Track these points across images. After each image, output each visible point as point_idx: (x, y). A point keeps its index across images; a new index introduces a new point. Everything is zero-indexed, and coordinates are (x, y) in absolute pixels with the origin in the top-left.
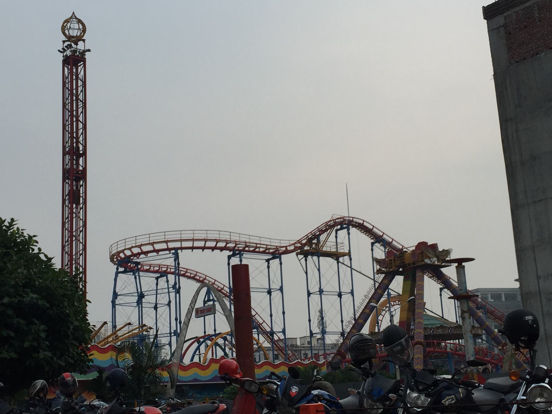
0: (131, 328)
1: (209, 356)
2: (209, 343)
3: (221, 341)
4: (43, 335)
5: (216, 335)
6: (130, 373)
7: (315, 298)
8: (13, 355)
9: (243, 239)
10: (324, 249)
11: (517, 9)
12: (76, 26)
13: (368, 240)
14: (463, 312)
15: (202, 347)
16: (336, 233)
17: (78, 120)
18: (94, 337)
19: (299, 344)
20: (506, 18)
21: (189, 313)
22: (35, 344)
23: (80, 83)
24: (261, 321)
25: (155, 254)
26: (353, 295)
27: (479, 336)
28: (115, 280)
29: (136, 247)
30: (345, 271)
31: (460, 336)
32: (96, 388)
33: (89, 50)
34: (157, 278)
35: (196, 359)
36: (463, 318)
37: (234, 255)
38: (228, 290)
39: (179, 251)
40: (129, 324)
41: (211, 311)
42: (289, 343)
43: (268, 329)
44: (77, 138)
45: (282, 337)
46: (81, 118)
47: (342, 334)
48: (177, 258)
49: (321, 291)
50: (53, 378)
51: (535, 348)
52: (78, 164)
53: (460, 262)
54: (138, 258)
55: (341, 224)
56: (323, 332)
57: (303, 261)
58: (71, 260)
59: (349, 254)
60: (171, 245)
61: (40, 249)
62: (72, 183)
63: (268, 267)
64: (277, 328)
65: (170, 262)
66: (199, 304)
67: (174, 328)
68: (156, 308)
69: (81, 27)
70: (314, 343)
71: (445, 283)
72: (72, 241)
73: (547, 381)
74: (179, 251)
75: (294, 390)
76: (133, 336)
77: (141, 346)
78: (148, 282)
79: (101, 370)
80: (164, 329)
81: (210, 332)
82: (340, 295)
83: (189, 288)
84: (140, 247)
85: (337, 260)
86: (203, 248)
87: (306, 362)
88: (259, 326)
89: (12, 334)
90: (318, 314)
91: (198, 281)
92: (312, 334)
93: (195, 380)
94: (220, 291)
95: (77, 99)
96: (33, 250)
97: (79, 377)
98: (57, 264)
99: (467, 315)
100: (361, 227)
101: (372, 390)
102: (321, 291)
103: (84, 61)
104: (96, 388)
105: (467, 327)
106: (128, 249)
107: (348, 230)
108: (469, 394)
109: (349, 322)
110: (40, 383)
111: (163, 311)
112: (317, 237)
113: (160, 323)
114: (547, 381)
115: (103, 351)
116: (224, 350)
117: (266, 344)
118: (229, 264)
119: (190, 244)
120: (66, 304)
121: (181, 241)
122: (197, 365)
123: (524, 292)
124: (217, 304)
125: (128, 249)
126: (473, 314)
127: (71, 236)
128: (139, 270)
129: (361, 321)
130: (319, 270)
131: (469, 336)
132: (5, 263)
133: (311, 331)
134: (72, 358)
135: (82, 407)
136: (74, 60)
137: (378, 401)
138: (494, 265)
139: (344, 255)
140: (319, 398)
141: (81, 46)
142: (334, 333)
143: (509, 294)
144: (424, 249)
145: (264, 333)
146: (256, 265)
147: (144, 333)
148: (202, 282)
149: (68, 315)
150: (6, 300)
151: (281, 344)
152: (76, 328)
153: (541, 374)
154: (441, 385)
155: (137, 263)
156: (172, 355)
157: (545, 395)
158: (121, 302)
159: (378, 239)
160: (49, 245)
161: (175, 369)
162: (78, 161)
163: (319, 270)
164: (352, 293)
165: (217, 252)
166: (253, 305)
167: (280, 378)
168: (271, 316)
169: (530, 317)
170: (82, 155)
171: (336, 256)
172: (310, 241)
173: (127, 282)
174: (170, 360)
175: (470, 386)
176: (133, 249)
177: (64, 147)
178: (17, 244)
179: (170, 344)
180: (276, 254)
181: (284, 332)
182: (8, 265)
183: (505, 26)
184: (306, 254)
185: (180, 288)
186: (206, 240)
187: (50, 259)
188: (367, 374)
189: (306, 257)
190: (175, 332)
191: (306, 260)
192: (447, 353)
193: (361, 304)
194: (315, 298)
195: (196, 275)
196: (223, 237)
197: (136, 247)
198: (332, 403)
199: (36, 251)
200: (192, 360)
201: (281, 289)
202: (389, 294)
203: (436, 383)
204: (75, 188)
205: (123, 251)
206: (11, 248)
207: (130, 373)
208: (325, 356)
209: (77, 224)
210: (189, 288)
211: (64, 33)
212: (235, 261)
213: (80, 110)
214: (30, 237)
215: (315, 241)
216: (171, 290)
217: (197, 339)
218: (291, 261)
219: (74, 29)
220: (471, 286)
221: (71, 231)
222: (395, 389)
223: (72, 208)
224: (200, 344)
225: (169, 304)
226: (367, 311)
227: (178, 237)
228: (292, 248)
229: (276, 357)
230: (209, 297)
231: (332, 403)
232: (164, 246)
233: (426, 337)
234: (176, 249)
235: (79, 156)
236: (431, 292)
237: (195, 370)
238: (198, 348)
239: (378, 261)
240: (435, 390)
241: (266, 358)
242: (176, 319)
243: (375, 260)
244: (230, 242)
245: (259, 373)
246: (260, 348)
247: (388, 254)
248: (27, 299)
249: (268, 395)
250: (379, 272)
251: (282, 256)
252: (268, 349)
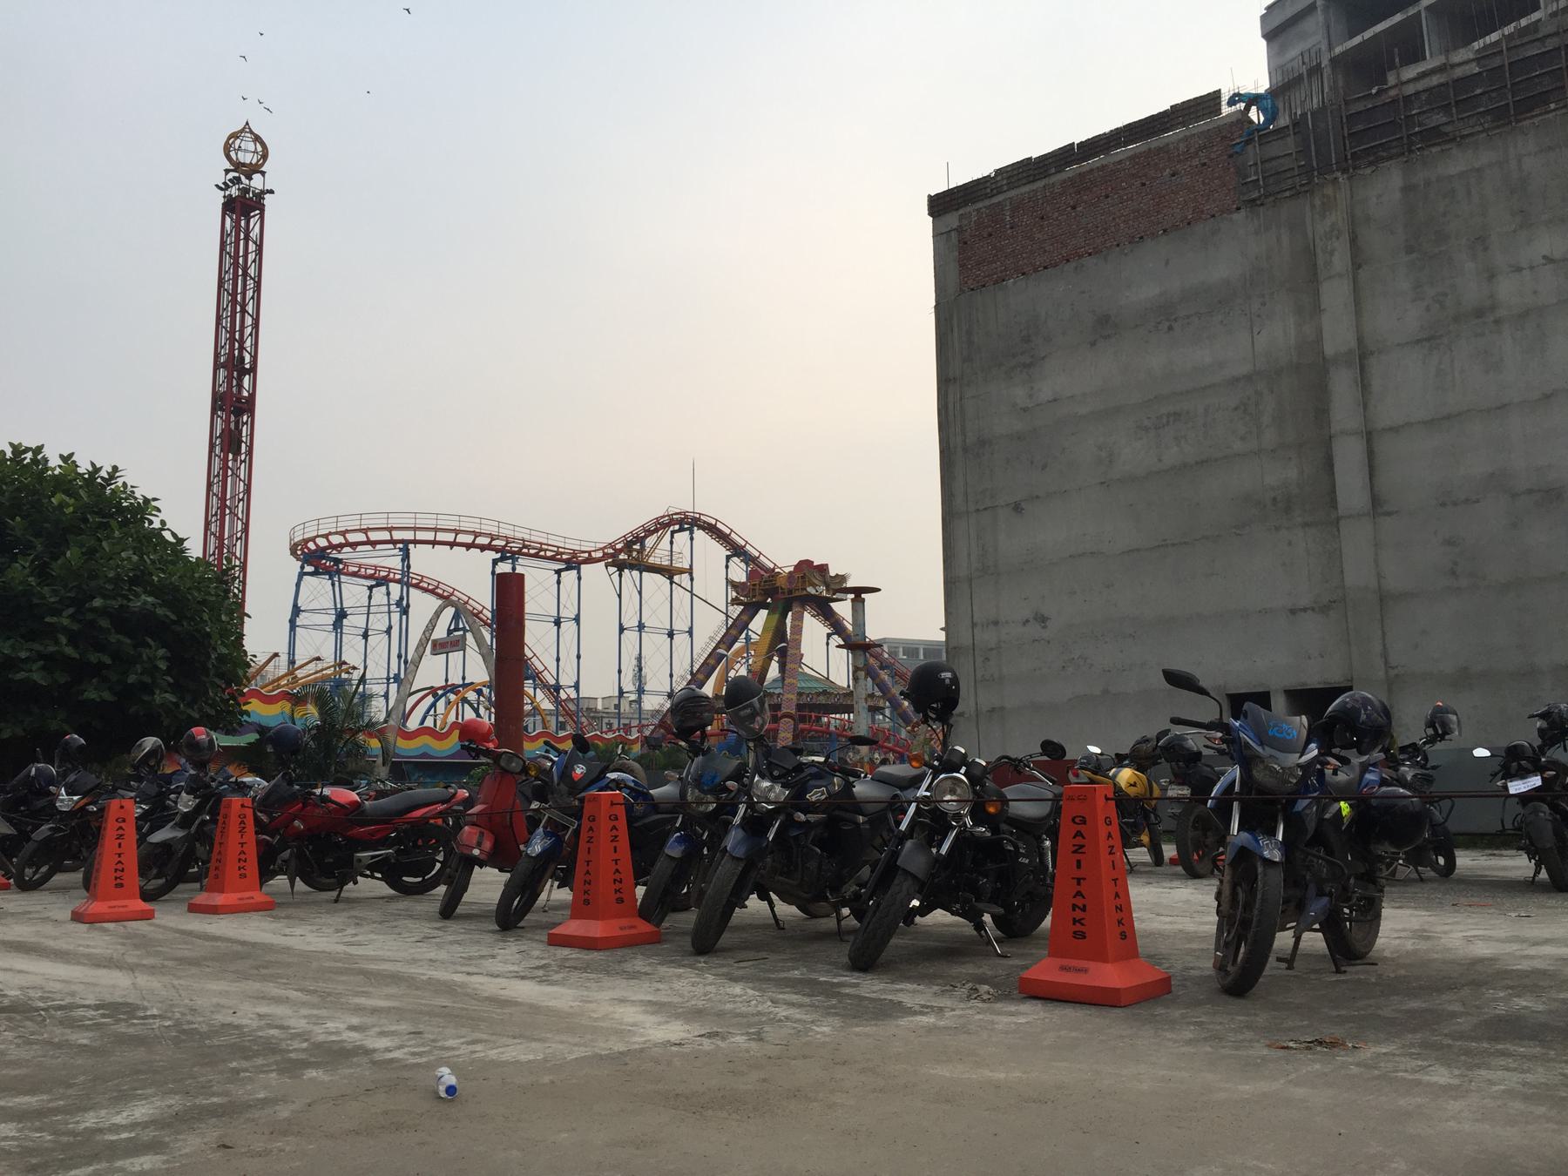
0: (320, 665)
1: (452, 718)
2: (452, 697)
3: (472, 696)
4: (163, 666)
5: (465, 686)
6: (314, 738)
7: (631, 637)
8: (107, 696)
10: (651, 560)
11: (980, 205)
12: (251, 146)
13: (722, 552)
14: (856, 669)
15: (441, 704)
17: (244, 311)
18: (254, 677)
19: (600, 707)
20: (961, 217)
21: (421, 646)
22: (147, 679)
23: (252, 247)
24: (541, 668)
25: (369, 547)
27: (880, 710)
28: (298, 585)
29: (360, 530)
30: (681, 596)
31: (849, 709)
32: (251, 758)
33: (271, 192)
34: (371, 588)
35: (429, 722)
36: (856, 679)
37: (502, 559)
38: (489, 615)
39: (411, 546)
40: (318, 659)
41: (459, 645)
42: (584, 705)
43: (552, 682)
44: (242, 342)
45: (573, 695)
46: (250, 308)
47: (670, 695)
48: (406, 556)
49: (641, 627)
50: (175, 738)
51: (951, 721)
52: (240, 386)
53: (859, 592)
55: (681, 522)
56: (641, 691)
57: (616, 577)
58: (220, 547)
59: (690, 571)
60: (397, 535)
61: (163, 523)
62: (228, 418)
63: (559, 582)
64: (567, 680)
65: (395, 562)
66: (440, 633)
67: (394, 670)
68: (365, 636)
69: (259, 148)
70: (625, 707)
71: (836, 626)
72: (223, 515)
73: (963, 770)
74: (411, 546)
75: (580, 770)
76: (325, 679)
77: (336, 698)
78: (354, 592)
79: (262, 730)
80: (377, 671)
81: (456, 679)
82: (671, 635)
83: (423, 605)
84: (343, 533)
85: (671, 578)
86: (452, 544)
87: (610, 736)
88: (536, 676)
89: (107, 660)
90: (635, 662)
91: (440, 596)
92: (621, 692)
93: (424, 755)
94: (476, 615)
95: (245, 274)
96: (151, 522)
97: (223, 740)
98: (195, 550)
99: (862, 674)
100: (713, 530)
101: (701, 776)
102: (641, 627)
103: (262, 209)
104: (251, 758)
105: (861, 693)
107: (692, 533)
108: (849, 786)
109: (683, 677)
110: (150, 742)
111: (378, 641)
112: (641, 540)
113: (373, 662)
114: (963, 770)
115: (268, 700)
116: (476, 711)
117: (547, 705)
118: (493, 573)
119: (430, 536)
120: (206, 617)
121: (415, 529)
122: (430, 732)
123: (951, 646)
124: (469, 636)
126: (870, 673)
127: (223, 507)
128: (339, 572)
129: (700, 676)
130: (640, 593)
131: (861, 705)
132: (100, 540)
134: (211, 706)
135: (221, 784)
136: (243, 206)
137: (710, 792)
138: (910, 609)
139: (681, 571)
140: (618, 784)
141: (257, 182)
142: (657, 693)
143: (930, 648)
144: (806, 569)
145: (545, 686)
146: (538, 580)
147: (344, 676)
148: (447, 599)
149: (208, 635)
150: (97, 602)
151: (572, 707)
152: (222, 659)
153: (956, 759)
154: (807, 771)
155: (338, 561)
156: (389, 714)
157: (959, 791)
158: (306, 622)
159: (737, 550)
160: (182, 517)
161: (391, 736)
162: (240, 381)
163: (640, 593)
164: (690, 632)
166: (528, 639)
167: (559, 752)
168: (558, 660)
169: (949, 675)
170: (248, 372)
171: (669, 572)
172: (628, 546)
173: (317, 590)
174: (386, 721)
175: (850, 773)
177: (217, 355)
178: (121, 510)
179: (386, 696)
180: (573, 562)
181: (577, 687)
182: (104, 544)
183: (959, 230)
184: (621, 567)
185: (408, 605)
186: (457, 532)
187: (181, 541)
188: (696, 750)
189: (621, 570)
190: (397, 678)
192: (830, 734)
193: (703, 650)
194: (631, 637)
196: (486, 529)
197: (360, 530)
198: (639, 793)
199: (157, 525)
200: (422, 722)
201: (577, 619)
202: (748, 638)
203: (800, 767)
204: (232, 426)
205: (313, 539)
206: (112, 516)
207: (314, 738)
208: (641, 728)
209: (234, 488)
210: (423, 605)
211: (228, 157)
212: (505, 568)
213: (249, 294)
214: (147, 501)
215: (637, 547)
216: (393, 608)
217: (433, 691)
218: (595, 573)
219: (246, 151)
220: (873, 633)
221: (223, 499)
222: (738, 775)
223: (226, 460)
224: (437, 698)
225: (389, 631)
226: (712, 662)
227: (410, 523)
228: (599, 554)
229: (562, 726)
230: (457, 624)
231: (639, 793)
232: (385, 536)
233: (799, 707)
234: (406, 542)
235: (243, 372)
236: (813, 633)
237: (426, 739)
238: (434, 705)
239: (734, 585)
240: (796, 779)
241: (545, 727)
242: (399, 656)
243: (729, 582)
244: (499, 537)
245: (533, 749)
246: (536, 710)
247: (750, 575)
248: (136, 604)
249: (537, 778)
250: (735, 602)
252: (550, 713)
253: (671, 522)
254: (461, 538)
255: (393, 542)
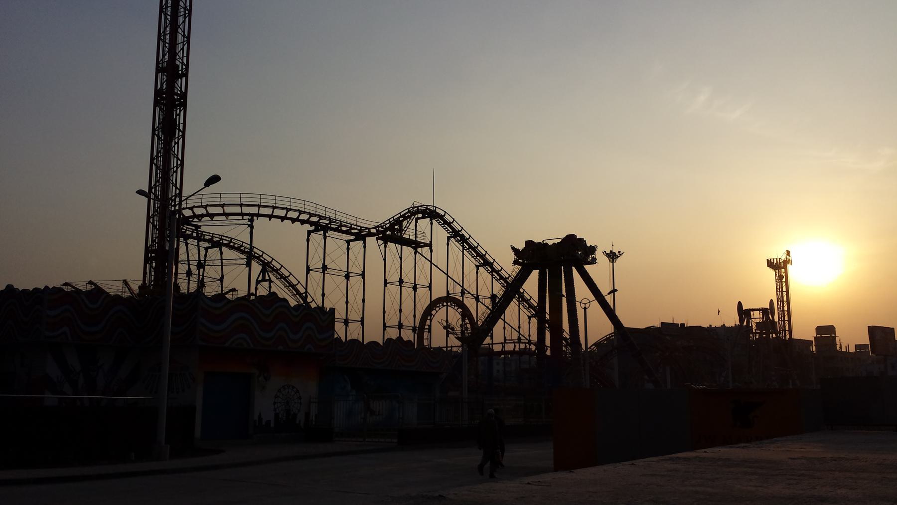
9: (338, 218)
16: (416, 222)
25: (224, 218)
26: (363, 278)
28: (308, 240)
29: (201, 206)
54: (200, 220)
57: (382, 247)
59: (430, 245)
60: (246, 210)
63: (348, 249)
74: (255, 218)
85: (415, 249)
86: (271, 217)
106: (189, 208)
121: (259, 206)
125: (189, 208)
133: (505, 338)
155: (197, 227)
165: (298, 224)
172: (392, 225)
176: (195, 210)
180: (361, 235)
184: (386, 240)
186: (288, 210)
191: (385, 247)
195: (242, 246)
197: (201, 206)
230: (264, 277)
232: (237, 210)
234: (252, 215)
244: (325, 218)
251: (367, 239)
253: (418, 212)
254: (277, 212)
255: (242, 214)
